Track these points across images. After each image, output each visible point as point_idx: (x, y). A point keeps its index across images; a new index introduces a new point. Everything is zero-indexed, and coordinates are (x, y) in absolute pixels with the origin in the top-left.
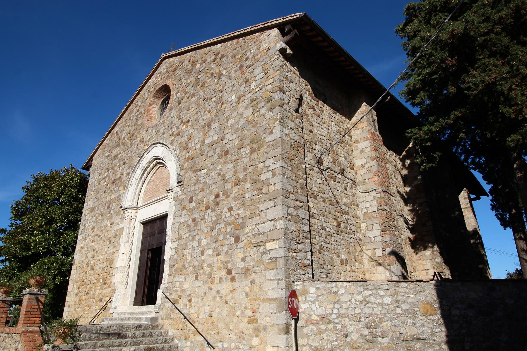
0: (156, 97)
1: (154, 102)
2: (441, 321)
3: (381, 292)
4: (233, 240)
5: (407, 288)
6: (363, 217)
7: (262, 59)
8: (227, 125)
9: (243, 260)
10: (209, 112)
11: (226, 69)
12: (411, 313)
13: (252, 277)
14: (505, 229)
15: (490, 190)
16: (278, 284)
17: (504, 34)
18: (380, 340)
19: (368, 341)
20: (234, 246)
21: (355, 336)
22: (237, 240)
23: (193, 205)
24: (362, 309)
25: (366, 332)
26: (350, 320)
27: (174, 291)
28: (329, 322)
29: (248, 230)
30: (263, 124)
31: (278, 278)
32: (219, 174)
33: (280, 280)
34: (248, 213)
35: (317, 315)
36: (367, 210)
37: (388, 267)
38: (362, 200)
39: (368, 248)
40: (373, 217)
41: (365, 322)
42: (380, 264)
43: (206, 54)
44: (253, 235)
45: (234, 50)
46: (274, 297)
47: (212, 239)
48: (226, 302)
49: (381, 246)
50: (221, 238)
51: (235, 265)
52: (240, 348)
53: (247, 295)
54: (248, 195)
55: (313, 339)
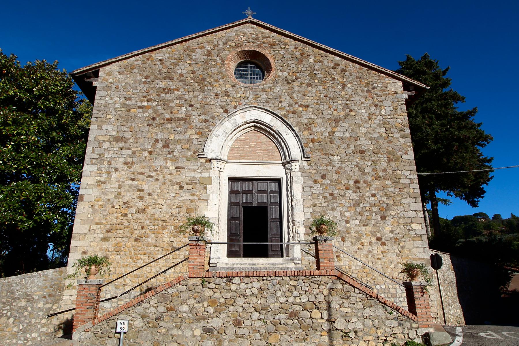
0: (238, 55)
9: (392, 232)
15: (494, 215)
22: (383, 218)
33: (425, 248)
34: (392, 202)
48: (379, 259)
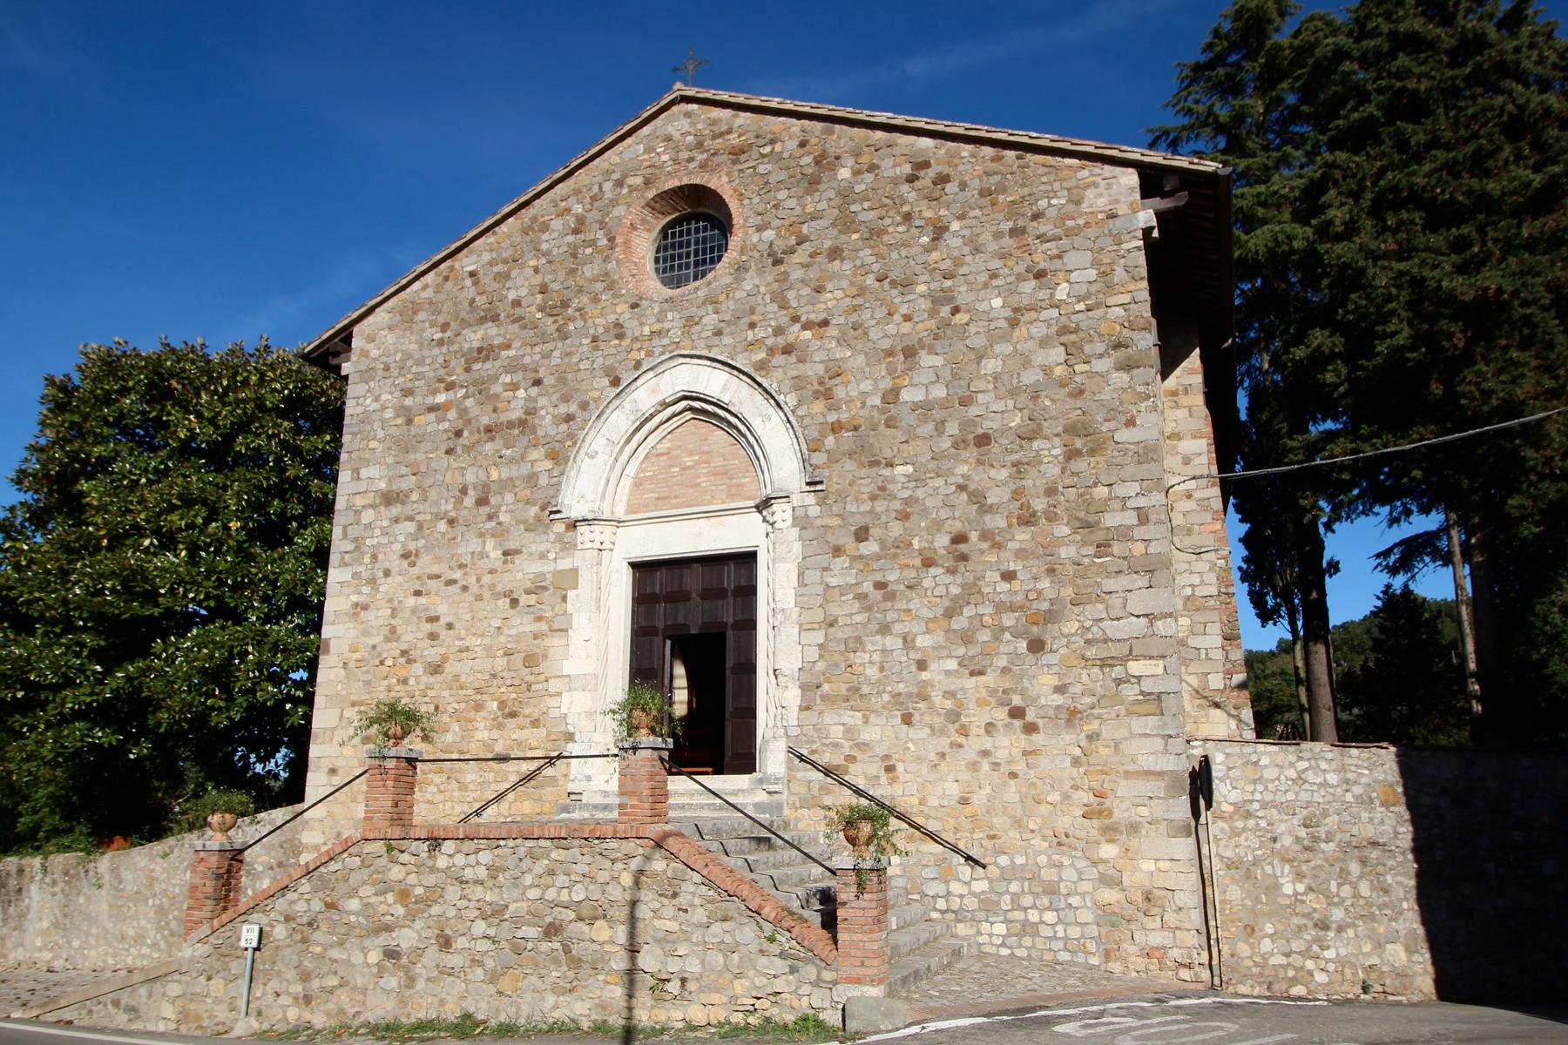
0: (654, 209)
1: (643, 221)
2: (1407, 816)
3: (1323, 765)
4: (1025, 645)
5: (1358, 758)
6: (1185, 604)
7: (1091, 233)
8: (978, 371)
9: (1060, 690)
10: (907, 318)
11: (961, 217)
12: (1365, 801)
13: (1090, 727)
14: (1263, 626)
16: (1166, 745)
17: (1553, 313)
18: (1323, 845)
19: (1306, 849)
20: (1031, 658)
21: (1287, 841)
22: (1036, 646)
23: (870, 547)
24: (1297, 794)
25: (1302, 833)
26: (1280, 813)
27: (824, 745)
28: (1248, 815)
29: (1070, 627)
30: (1103, 397)
31: (1167, 732)
32: (962, 488)
33: (1170, 736)
35: (1231, 804)
36: (1193, 591)
37: (1234, 712)
38: (1182, 567)
39: (1190, 670)
40: (1205, 608)
41: (1301, 816)
42: (1217, 705)
43: (872, 149)
44: (1088, 642)
45: (987, 174)
46: (1158, 768)
47: (951, 636)
48: (1013, 775)
49: (1222, 669)
50: (984, 636)
51: (1035, 700)
52: (1066, 863)
53: (1076, 762)
54: (1065, 552)
55: (1226, 846)
